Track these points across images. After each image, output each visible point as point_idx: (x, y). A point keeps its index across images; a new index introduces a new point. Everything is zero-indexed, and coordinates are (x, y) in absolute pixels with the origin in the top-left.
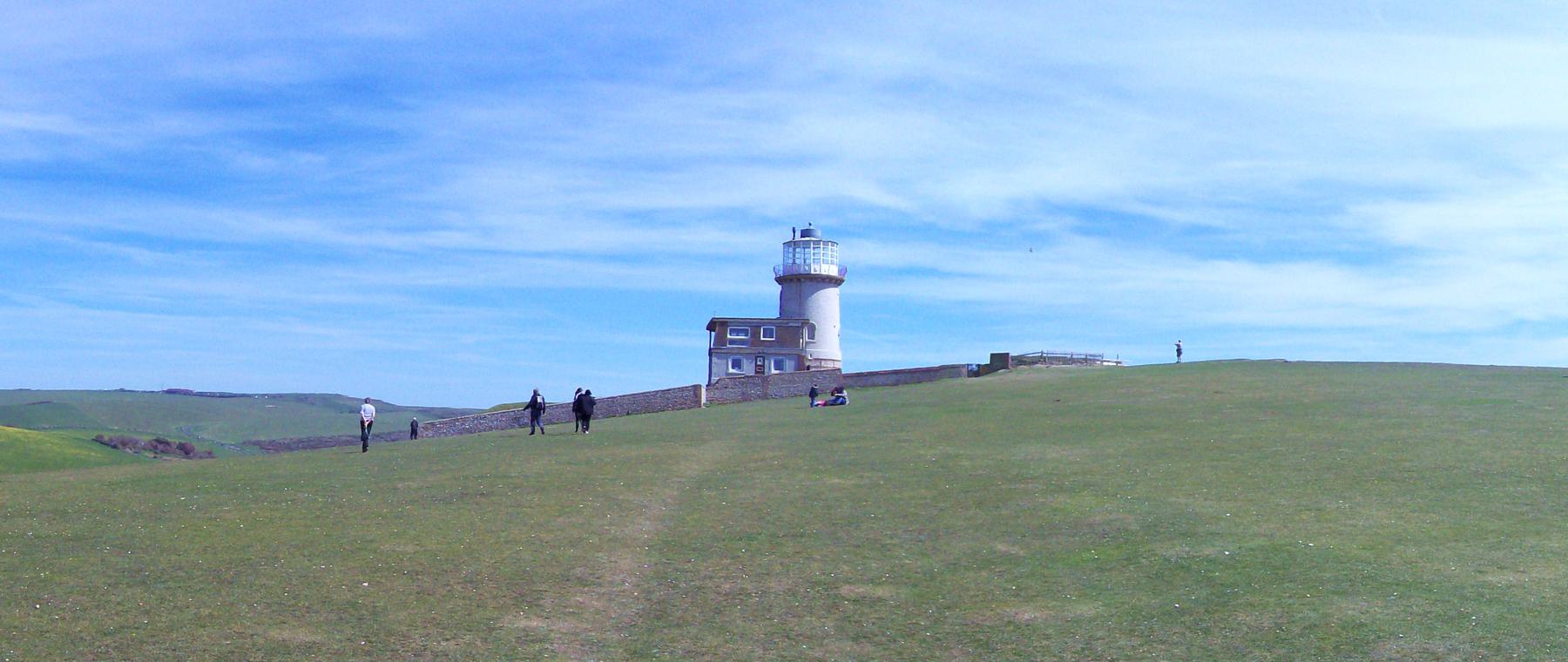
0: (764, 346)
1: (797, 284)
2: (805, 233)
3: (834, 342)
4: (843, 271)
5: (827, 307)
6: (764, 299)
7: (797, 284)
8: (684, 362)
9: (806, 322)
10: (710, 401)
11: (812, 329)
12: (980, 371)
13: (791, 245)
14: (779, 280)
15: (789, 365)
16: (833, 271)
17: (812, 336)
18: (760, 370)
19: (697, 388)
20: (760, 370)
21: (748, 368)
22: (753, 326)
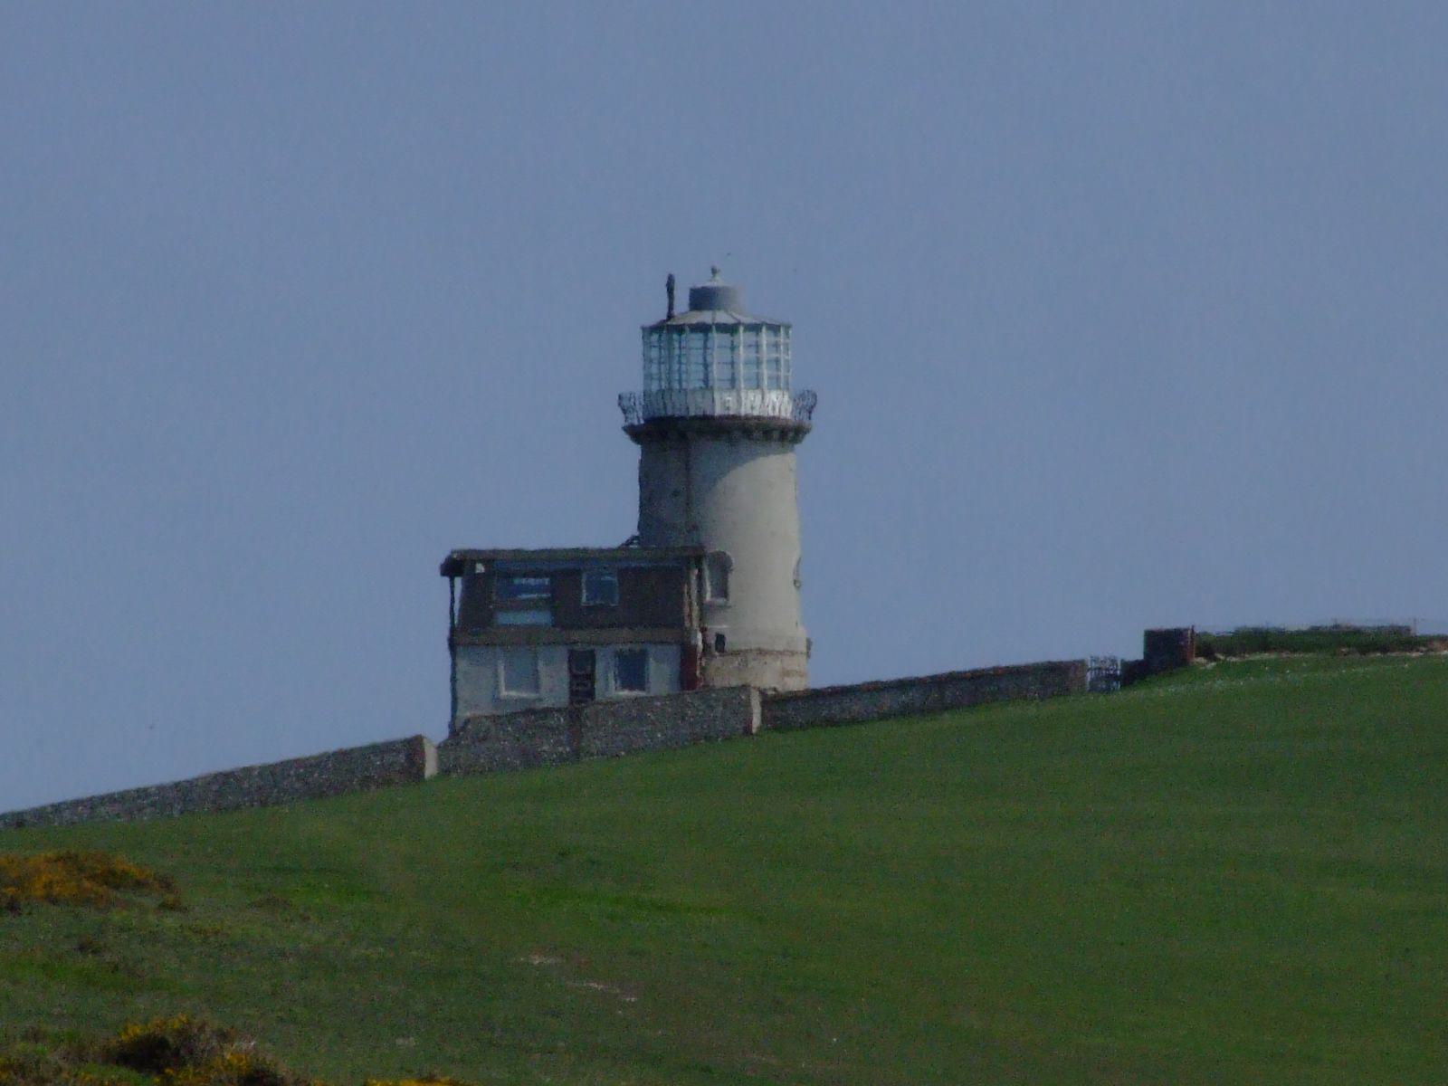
0: (601, 618)
1: (750, 346)
2: (702, 298)
3: (814, 595)
4: (807, 402)
5: (767, 512)
6: (593, 505)
7: (680, 442)
8: (395, 681)
9: (697, 557)
10: (445, 771)
11: (723, 566)
12: (1133, 674)
13: (666, 330)
14: (634, 433)
15: (660, 675)
16: (775, 404)
17: (723, 591)
18: (582, 685)
19: (413, 747)
20: (582, 685)
21: (553, 685)
22: (562, 574)
